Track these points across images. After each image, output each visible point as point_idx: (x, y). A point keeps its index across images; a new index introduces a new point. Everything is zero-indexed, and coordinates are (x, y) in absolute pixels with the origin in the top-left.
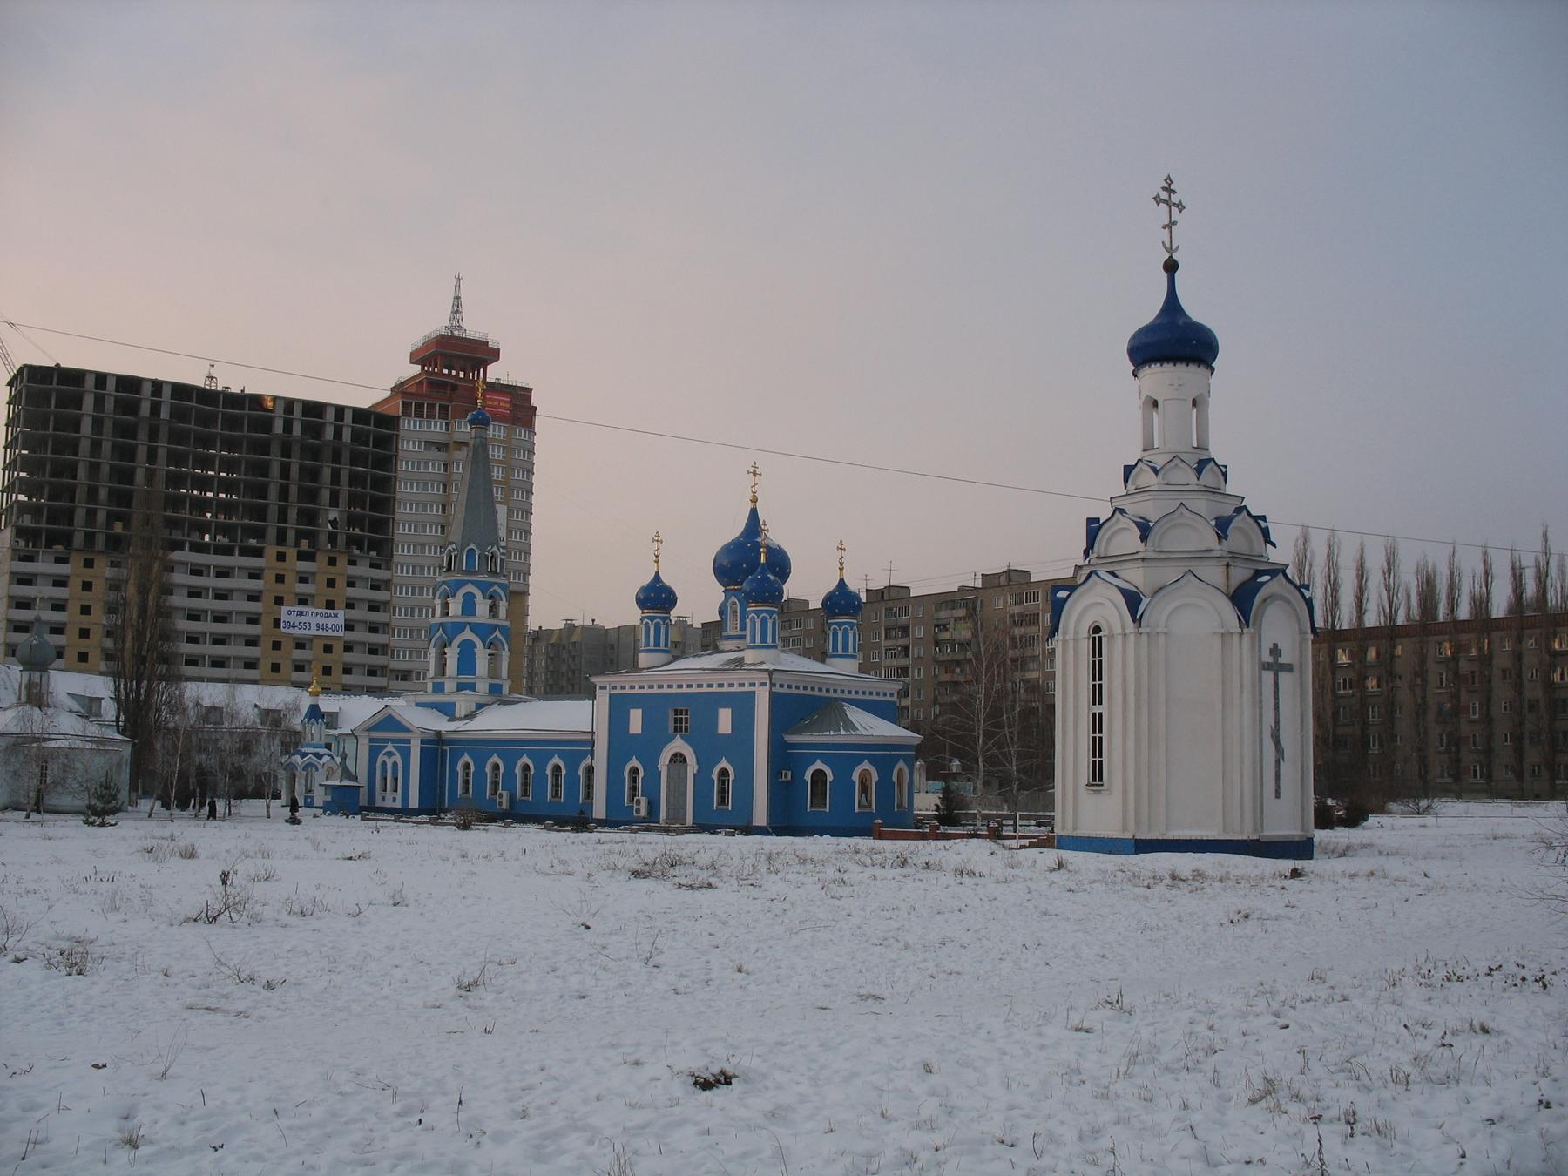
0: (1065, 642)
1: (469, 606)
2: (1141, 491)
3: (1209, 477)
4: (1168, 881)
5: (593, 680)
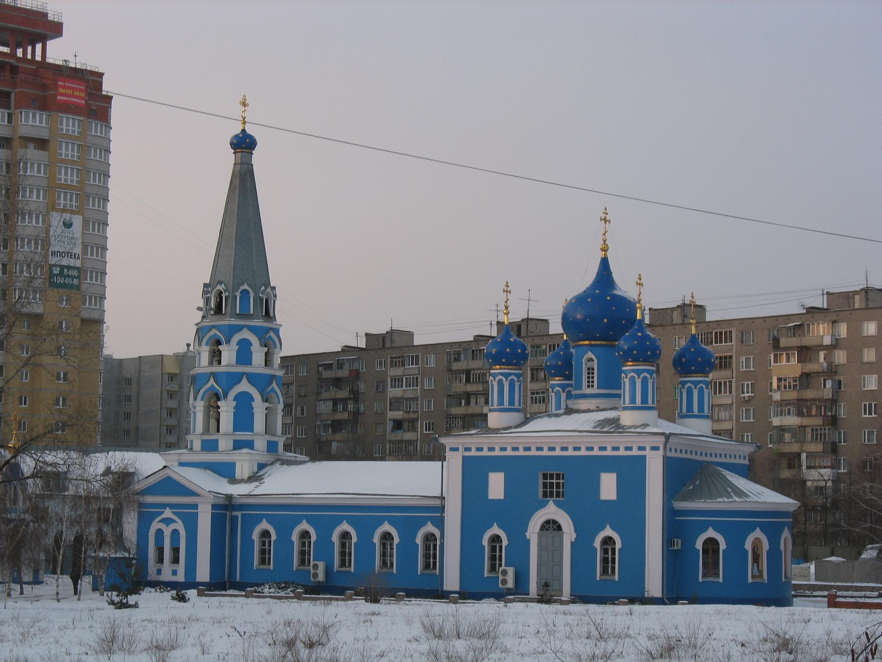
1: (244, 355)
5: (443, 440)
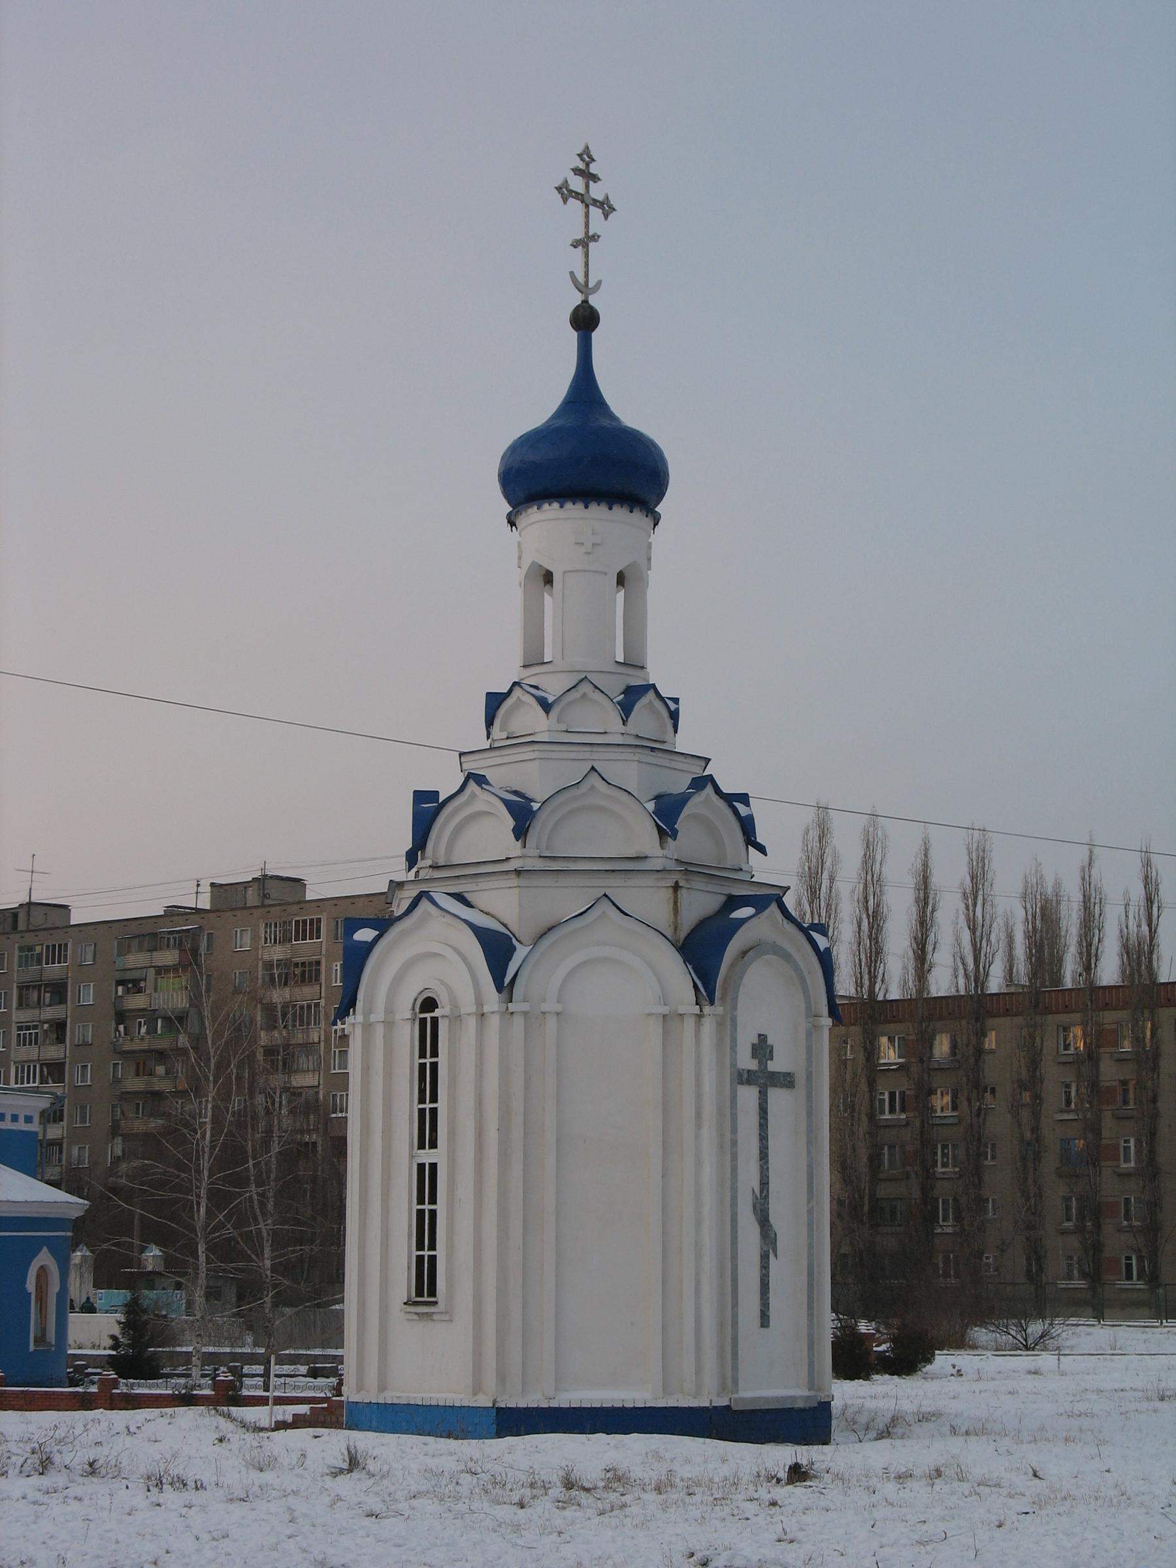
0: (368, 1027)
2: (517, 742)
3: (644, 719)
4: (557, 1491)
